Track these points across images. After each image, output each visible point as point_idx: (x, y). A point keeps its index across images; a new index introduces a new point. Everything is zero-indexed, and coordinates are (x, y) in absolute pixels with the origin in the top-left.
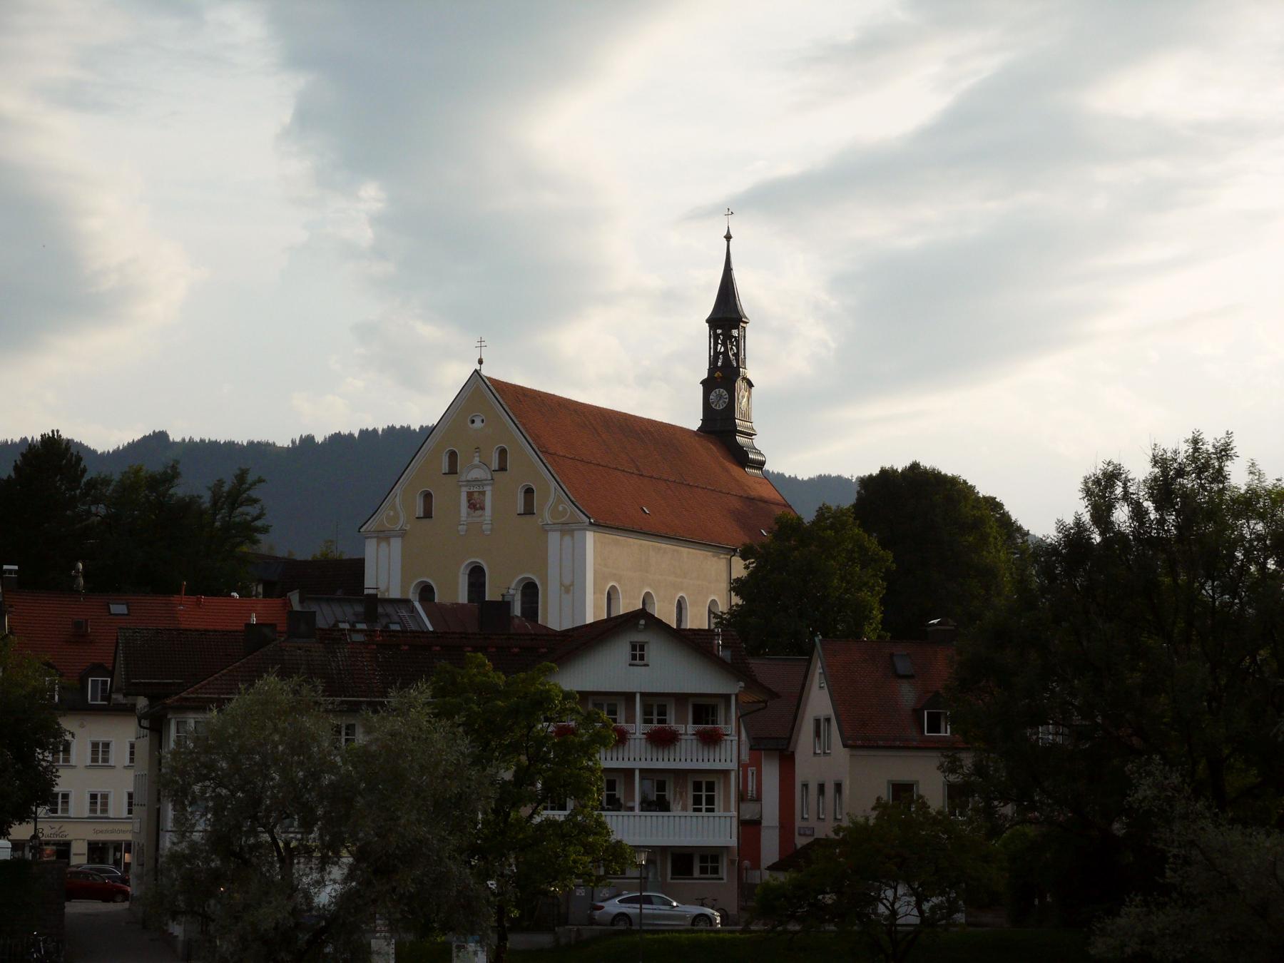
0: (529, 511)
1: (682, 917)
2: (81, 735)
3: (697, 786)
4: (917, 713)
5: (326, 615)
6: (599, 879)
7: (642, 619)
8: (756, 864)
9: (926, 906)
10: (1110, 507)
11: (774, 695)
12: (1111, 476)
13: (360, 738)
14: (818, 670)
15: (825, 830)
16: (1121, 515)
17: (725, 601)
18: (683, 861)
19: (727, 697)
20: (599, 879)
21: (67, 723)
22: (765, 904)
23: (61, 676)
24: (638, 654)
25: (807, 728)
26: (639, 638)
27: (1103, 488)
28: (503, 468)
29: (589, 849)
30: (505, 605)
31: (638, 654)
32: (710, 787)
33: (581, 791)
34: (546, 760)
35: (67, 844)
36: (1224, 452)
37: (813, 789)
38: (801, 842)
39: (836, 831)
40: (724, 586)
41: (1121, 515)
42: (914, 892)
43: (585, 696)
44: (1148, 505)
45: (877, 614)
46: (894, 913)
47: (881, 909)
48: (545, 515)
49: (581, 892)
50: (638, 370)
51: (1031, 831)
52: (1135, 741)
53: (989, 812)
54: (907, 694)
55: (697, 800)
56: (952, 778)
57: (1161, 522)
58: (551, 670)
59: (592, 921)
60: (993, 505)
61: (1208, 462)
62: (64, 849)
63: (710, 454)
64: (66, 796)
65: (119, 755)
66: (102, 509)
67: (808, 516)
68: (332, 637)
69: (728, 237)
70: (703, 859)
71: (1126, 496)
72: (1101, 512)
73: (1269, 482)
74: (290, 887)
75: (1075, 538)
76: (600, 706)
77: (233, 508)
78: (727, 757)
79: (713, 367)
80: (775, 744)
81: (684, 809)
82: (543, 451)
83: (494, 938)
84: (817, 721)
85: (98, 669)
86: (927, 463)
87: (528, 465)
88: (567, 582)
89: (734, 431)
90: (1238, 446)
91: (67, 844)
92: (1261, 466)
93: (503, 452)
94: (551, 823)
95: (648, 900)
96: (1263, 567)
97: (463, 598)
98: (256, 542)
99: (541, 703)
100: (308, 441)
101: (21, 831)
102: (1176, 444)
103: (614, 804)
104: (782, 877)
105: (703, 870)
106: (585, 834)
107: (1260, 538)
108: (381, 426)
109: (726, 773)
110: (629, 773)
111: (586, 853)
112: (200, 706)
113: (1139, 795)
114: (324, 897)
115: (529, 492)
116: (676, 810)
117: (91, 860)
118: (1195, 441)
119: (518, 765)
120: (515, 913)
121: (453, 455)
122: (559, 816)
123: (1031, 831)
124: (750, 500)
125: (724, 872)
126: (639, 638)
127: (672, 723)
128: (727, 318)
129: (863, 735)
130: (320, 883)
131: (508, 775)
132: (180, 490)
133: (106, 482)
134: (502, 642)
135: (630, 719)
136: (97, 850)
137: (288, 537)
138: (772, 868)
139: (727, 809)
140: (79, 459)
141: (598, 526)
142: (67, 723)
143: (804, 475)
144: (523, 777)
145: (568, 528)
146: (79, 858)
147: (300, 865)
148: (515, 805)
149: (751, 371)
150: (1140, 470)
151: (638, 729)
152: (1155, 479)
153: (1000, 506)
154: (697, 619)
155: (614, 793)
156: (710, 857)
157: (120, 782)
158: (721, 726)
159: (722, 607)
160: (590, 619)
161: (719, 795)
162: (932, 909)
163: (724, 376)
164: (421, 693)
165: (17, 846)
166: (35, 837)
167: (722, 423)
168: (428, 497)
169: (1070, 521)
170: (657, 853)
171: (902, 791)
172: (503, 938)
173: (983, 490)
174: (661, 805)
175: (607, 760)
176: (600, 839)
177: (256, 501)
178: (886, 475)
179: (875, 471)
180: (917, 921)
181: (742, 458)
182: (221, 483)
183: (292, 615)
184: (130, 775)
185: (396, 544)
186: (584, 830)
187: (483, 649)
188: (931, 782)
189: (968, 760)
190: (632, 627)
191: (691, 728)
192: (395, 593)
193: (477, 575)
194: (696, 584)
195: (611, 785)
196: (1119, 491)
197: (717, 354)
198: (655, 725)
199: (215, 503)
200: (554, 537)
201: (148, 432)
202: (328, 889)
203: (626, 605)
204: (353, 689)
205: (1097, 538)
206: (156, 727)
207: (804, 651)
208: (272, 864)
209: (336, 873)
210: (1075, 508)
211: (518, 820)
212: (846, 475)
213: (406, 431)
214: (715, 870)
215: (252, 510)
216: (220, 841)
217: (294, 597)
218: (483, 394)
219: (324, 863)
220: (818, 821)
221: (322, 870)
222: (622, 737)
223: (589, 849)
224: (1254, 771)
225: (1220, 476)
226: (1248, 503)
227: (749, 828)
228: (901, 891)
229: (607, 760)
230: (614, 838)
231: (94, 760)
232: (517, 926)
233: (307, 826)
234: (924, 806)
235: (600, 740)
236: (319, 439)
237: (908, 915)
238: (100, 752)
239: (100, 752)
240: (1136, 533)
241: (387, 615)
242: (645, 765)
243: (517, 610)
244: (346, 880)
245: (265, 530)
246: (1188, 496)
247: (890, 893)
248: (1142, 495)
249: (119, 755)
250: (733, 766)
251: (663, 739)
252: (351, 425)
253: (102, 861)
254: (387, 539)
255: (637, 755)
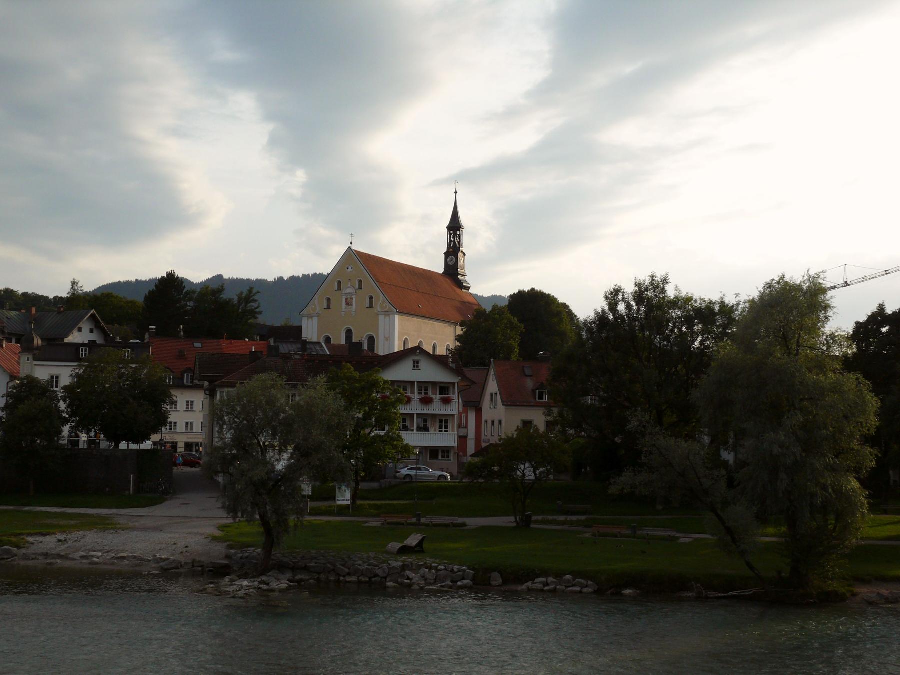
0: (371, 306)
1: (434, 476)
2: (181, 398)
3: (441, 421)
4: (534, 391)
5: (284, 348)
6: (399, 460)
7: (418, 350)
8: (465, 455)
9: (538, 472)
10: (616, 304)
11: (474, 383)
12: (617, 291)
13: (298, 399)
14: (492, 372)
15: (495, 440)
16: (622, 307)
17: (453, 344)
18: (434, 453)
19: (454, 384)
20: (399, 460)
21: (174, 392)
22: (469, 471)
23: (172, 372)
24: (416, 365)
25: (487, 398)
26: (417, 358)
27: (613, 297)
28: (360, 288)
29: (395, 447)
30: (360, 344)
31: (416, 365)
32: (446, 422)
33: (391, 422)
34: (377, 409)
35: (177, 443)
36: (665, 281)
37: (490, 423)
38: (484, 445)
39: (500, 440)
40: (453, 338)
41: (622, 307)
42: (533, 466)
43: (393, 382)
44: (633, 303)
45: (517, 350)
46: (524, 475)
47: (519, 473)
48: (378, 307)
49: (391, 465)
50: (415, 246)
51: (582, 441)
52: (627, 404)
53: (564, 432)
54: (530, 384)
55: (441, 427)
56: (549, 418)
57: (639, 310)
58: (379, 371)
59: (396, 478)
60: (565, 306)
61: (658, 286)
62: (175, 446)
63: (447, 283)
64: (175, 423)
65: (198, 406)
66: (191, 304)
67: (489, 309)
68: (287, 357)
69: (456, 193)
70: (443, 452)
71: (624, 300)
72: (613, 306)
73: (683, 294)
74: (266, 463)
75: (601, 318)
76: (400, 387)
77: (247, 304)
78: (454, 409)
79: (449, 247)
80: (474, 404)
81: (435, 431)
82: (377, 281)
83: (353, 484)
84: (492, 395)
85: (188, 370)
86: (538, 288)
87: (369, 281)
88: (387, 336)
89: (457, 274)
90: (671, 279)
91: (177, 443)
92: (680, 287)
93: (360, 282)
94: (378, 436)
95: (420, 469)
96: (681, 330)
97: (343, 342)
98: (256, 318)
99: (374, 385)
100: (281, 279)
101: (156, 437)
102: (645, 279)
103: (406, 428)
104: (476, 460)
105: (443, 457)
106: (393, 441)
107: (679, 318)
108: (311, 273)
109: (453, 416)
110: (412, 415)
111: (394, 449)
112: (233, 386)
113: (631, 426)
114: (280, 466)
115: (371, 298)
116: (432, 431)
117: (186, 450)
118: (653, 277)
119: (365, 411)
120: (363, 474)
121: (339, 283)
122: (382, 433)
123: (582, 441)
124: (464, 303)
125: (452, 457)
126: (417, 358)
127: (430, 395)
128: (455, 226)
129: (511, 400)
130: (279, 461)
131: (360, 416)
132: (225, 296)
133: (194, 292)
134: (358, 361)
135: (413, 393)
136: (189, 446)
137: (269, 317)
138: (472, 456)
139: (453, 431)
140: (182, 282)
141: (400, 313)
142: (174, 392)
143: (486, 295)
144: (367, 416)
145: (387, 314)
146: (181, 449)
147: (270, 453)
148: (363, 428)
149: (464, 249)
150: (629, 289)
151: (416, 397)
152: (636, 292)
153: (568, 307)
154: (441, 351)
155: (406, 423)
156: (446, 451)
157: (198, 418)
158: (451, 396)
159: (452, 347)
160: (396, 351)
161: (450, 426)
162: (540, 473)
163: (454, 251)
164: (322, 379)
165: (155, 443)
166: (161, 440)
167: (452, 271)
168: (329, 300)
169: (600, 310)
170: (424, 449)
171: (527, 424)
172: (357, 484)
173: (561, 300)
174: (426, 429)
175: (403, 410)
176: (399, 443)
177: (256, 301)
178: (521, 294)
179: (516, 292)
180: (534, 478)
181: (461, 285)
182: (242, 293)
183: (269, 347)
184: (202, 414)
185: (315, 320)
186: (393, 439)
187: (350, 363)
188: (539, 419)
189: (556, 411)
190: (414, 353)
191: (438, 397)
192: (315, 340)
193: (349, 333)
194: (442, 338)
195: (404, 421)
196: (620, 297)
197: (451, 242)
198: (423, 395)
199: (239, 301)
200: (381, 318)
201: (215, 275)
202: (281, 463)
203: (410, 345)
204: (295, 379)
205: (611, 317)
206: (212, 394)
207: (486, 366)
208: (258, 453)
209: (286, 456)
210: (602, 305)
211: (365, 435)
212: (503, 295)
213: (321, 275)
214: (448, 457)
215: (255, 305)
216: (238, 442)
217: (272, 341)
218: (352, 257)
219: (281, 452)
220: (492, 436)
221: (280, 455)
222: (409, 401)
223: (395, 447)
224: (675, 416)
225: (663, 291)
226: (675, 303)
227: (463, 439)
228: (527, 465)
229: (403, 410)
230: (405, 443)
231: (187, 408)
232: (364, 480)
233: (274, 436)
234: (537, 430)
235: (399, 401)
236: (286, 278)
237: (530, 475)
238: (190, 405)
239: (190, 405)
240: (628, 315)
241: (311, 349)
242: (419, 412)
243: (366, 347)
244: (290, 459)
245: (260, 313)
246: (650, 300)
247: (522, 467)
248: (631, 298)
249: (198, 406)
250: (456, 413)
251: (426, 401)
252: (299, 273)
253: (191, 451)
254: (312, 318)
255: (415, 408)
